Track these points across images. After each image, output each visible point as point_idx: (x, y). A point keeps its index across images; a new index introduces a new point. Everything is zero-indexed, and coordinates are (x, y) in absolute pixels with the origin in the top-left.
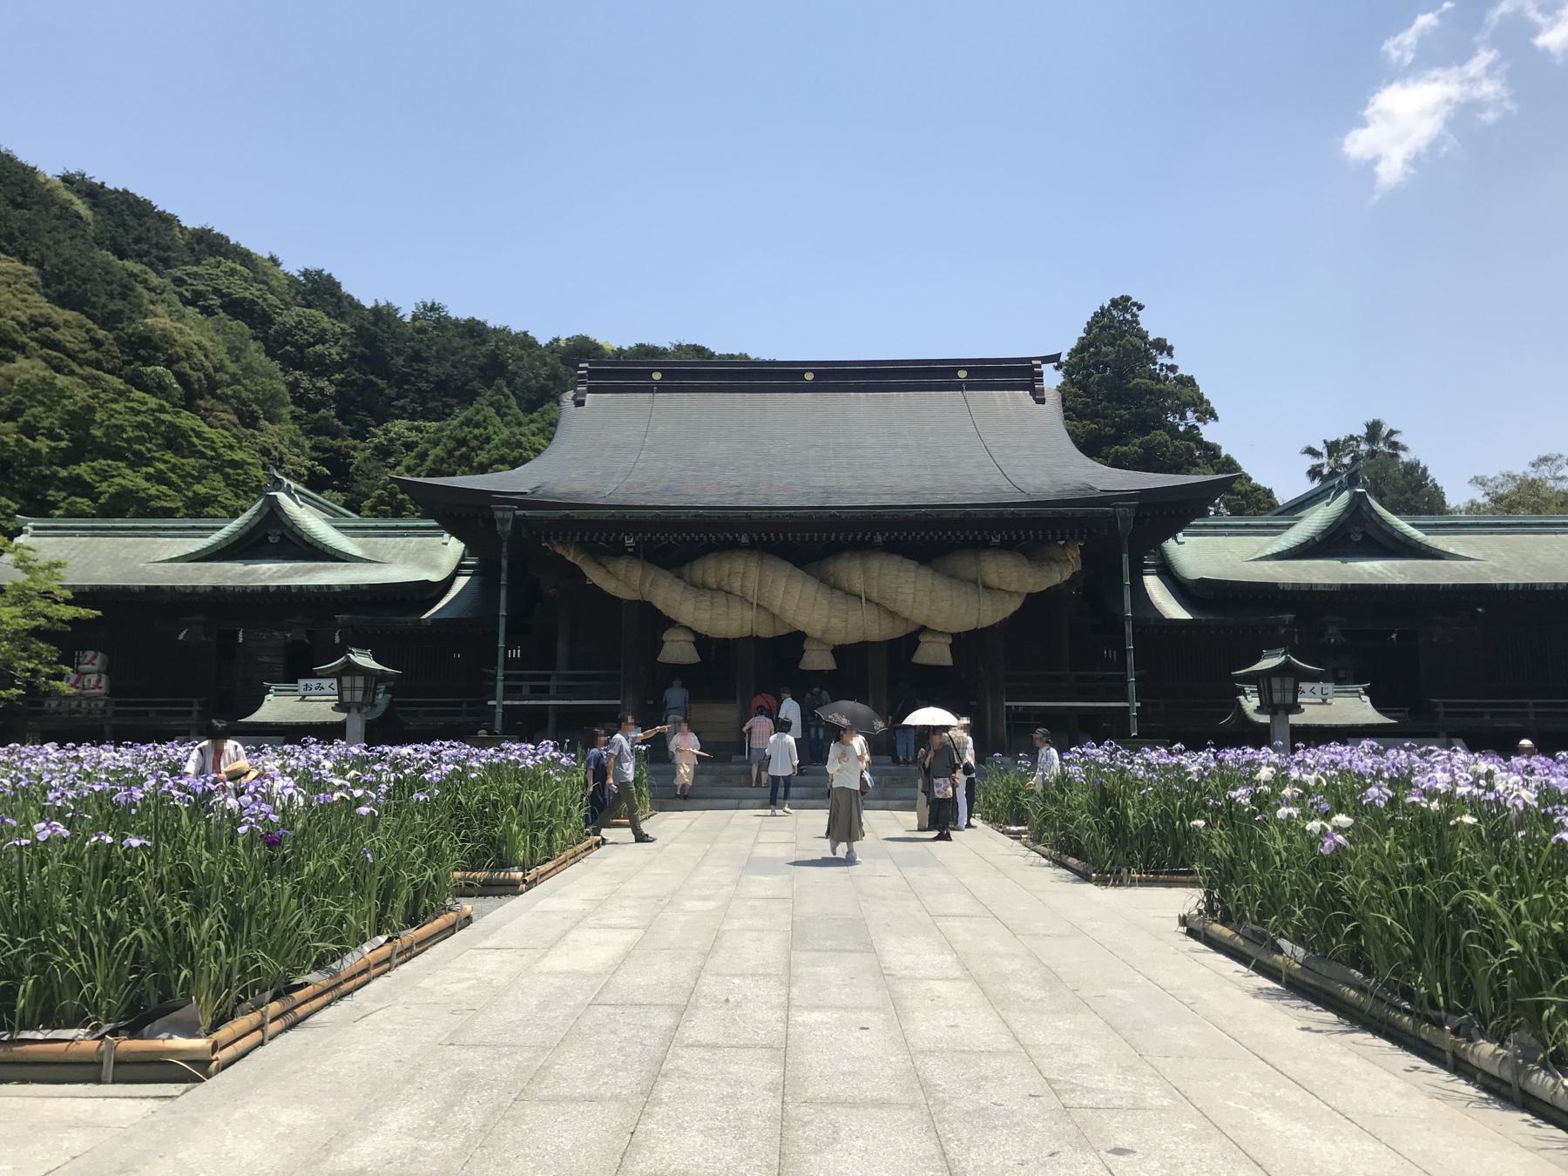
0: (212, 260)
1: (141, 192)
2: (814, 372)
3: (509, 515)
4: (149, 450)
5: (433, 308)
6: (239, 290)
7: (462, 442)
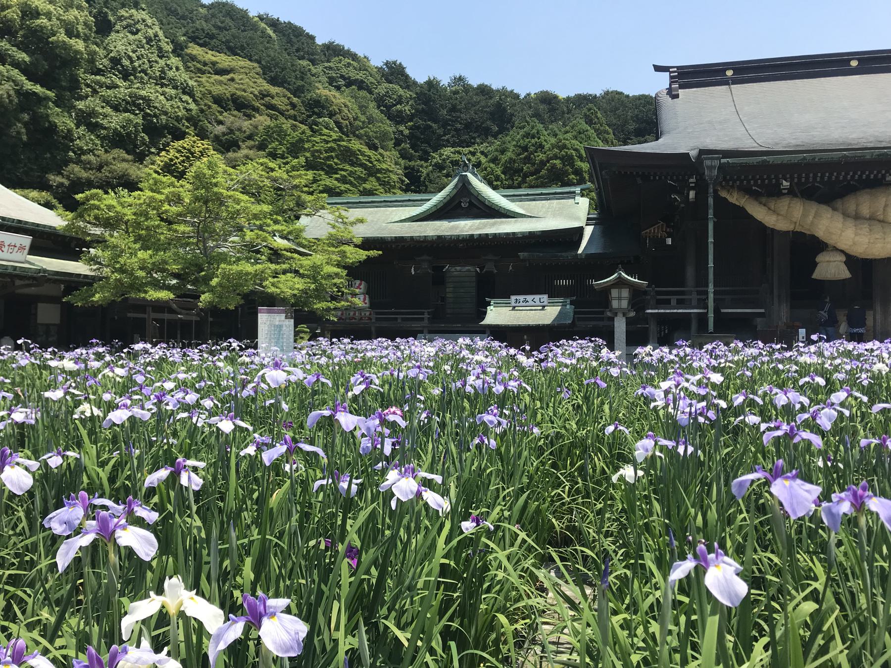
0: (337, 59)
1: (297, 23)
2: (858, 59)
3: (716, 163)
4: (336, 164)
5: (461, 79)
6: (354, 75)
7: (525, 149)
